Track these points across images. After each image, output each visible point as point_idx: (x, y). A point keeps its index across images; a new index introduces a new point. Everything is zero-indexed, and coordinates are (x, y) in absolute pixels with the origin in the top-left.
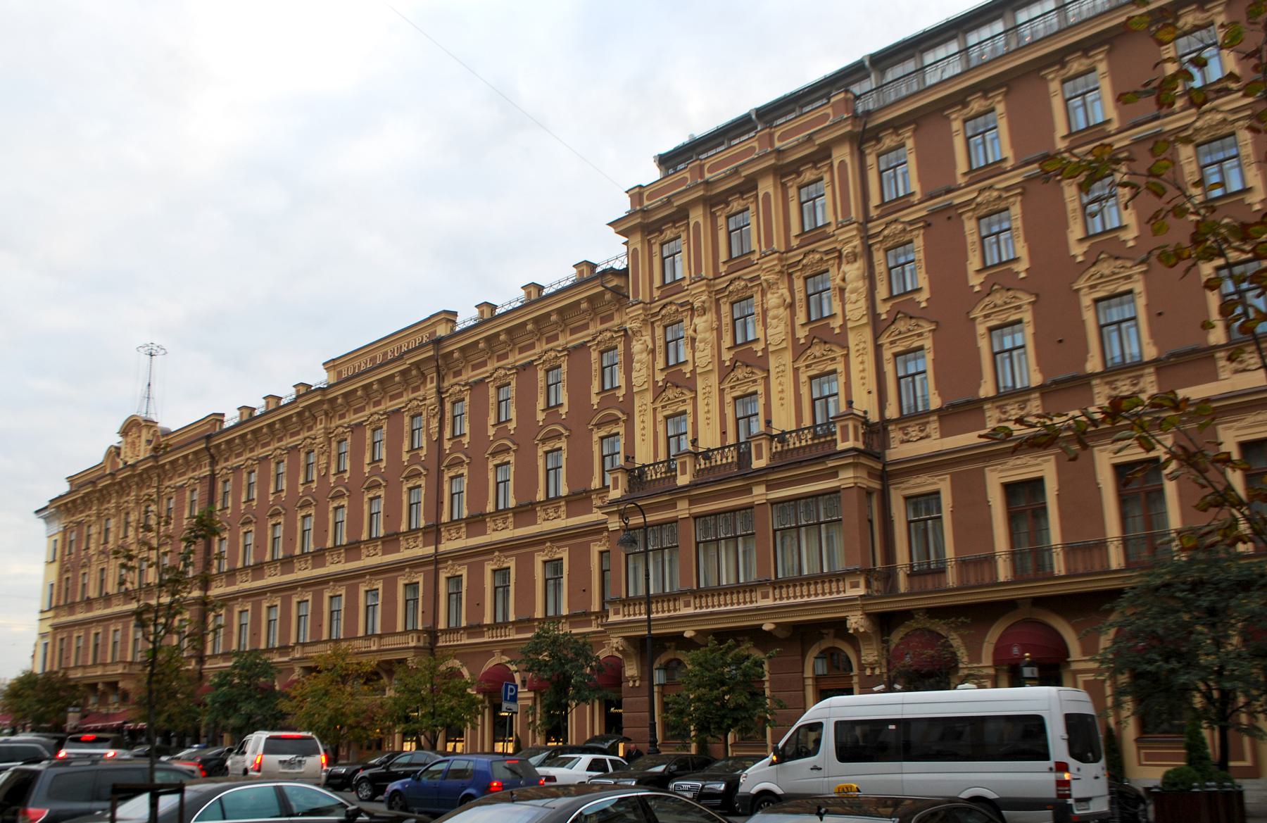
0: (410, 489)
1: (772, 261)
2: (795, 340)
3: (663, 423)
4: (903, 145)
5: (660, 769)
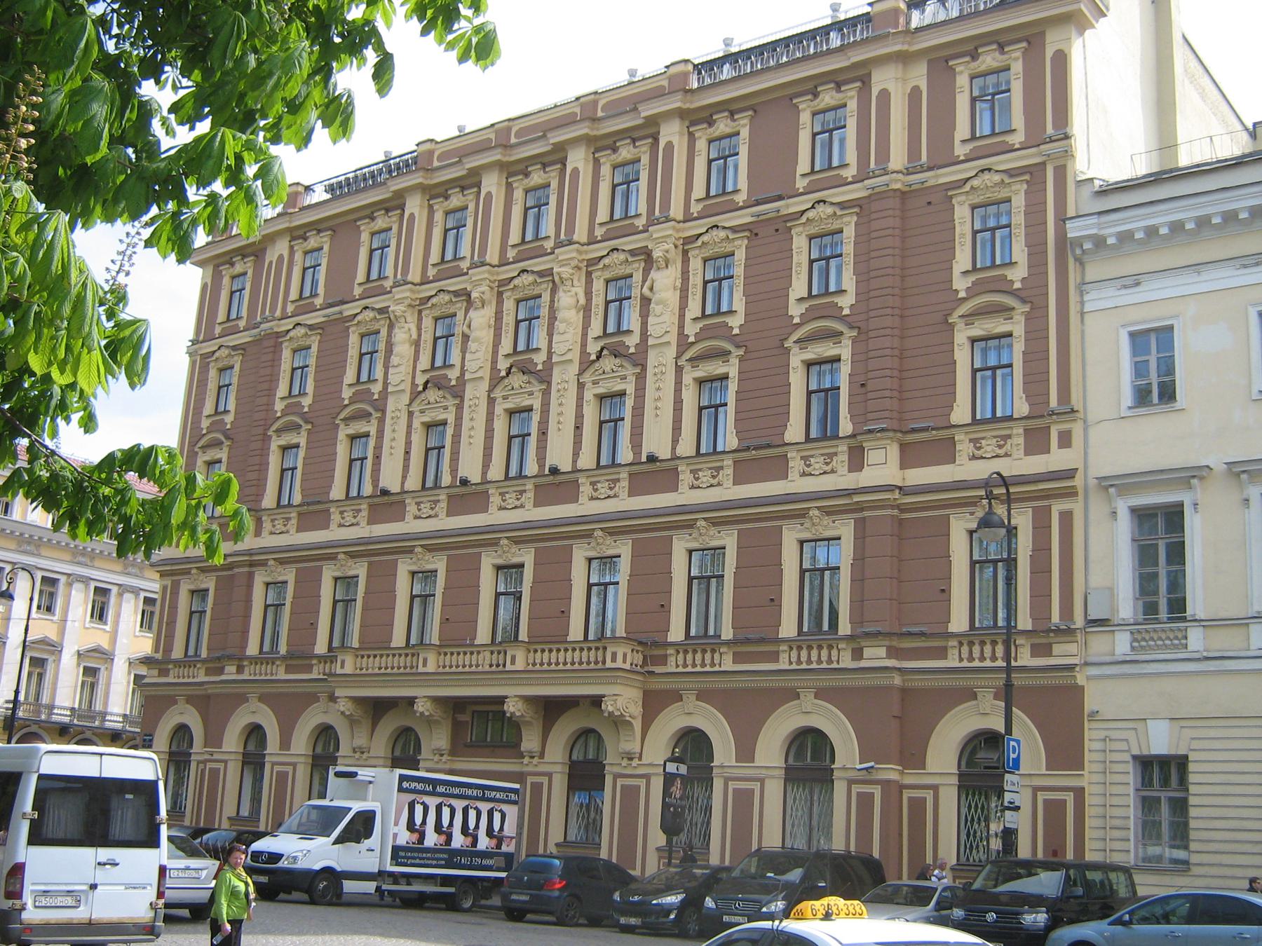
5: (636, 898)
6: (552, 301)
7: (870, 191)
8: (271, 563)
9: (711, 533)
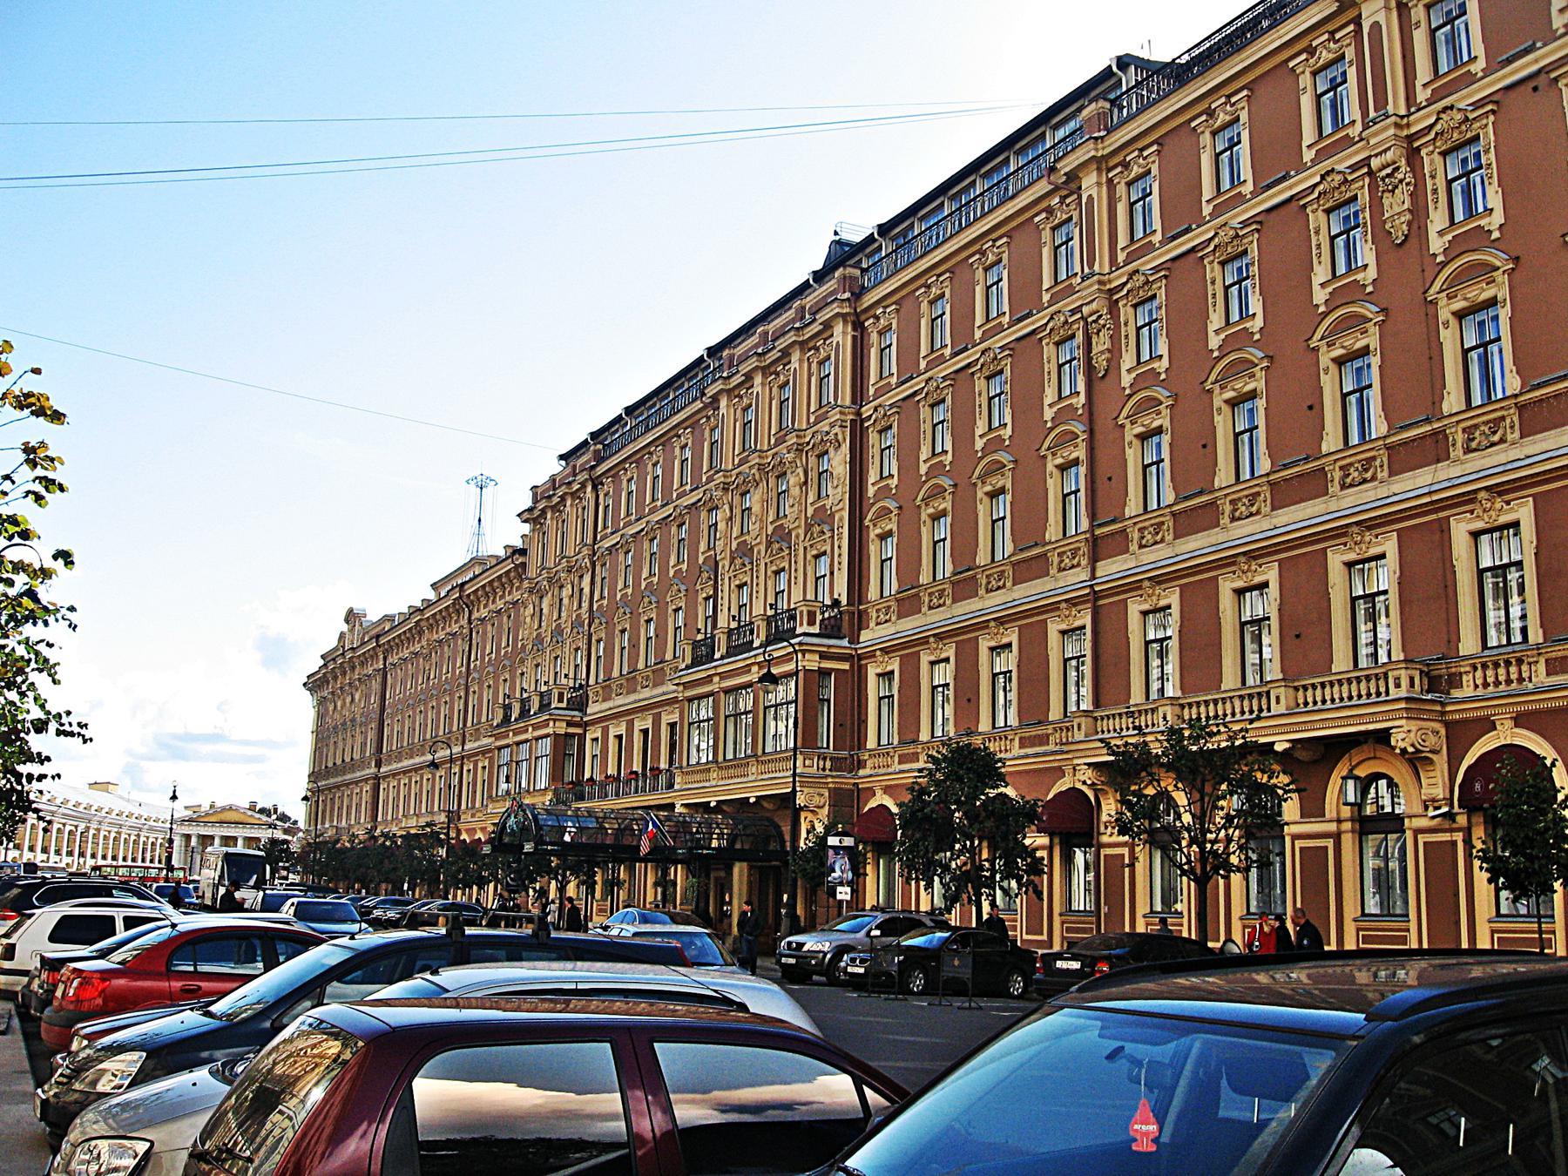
3: (929, 522)
9: (1498, 506)
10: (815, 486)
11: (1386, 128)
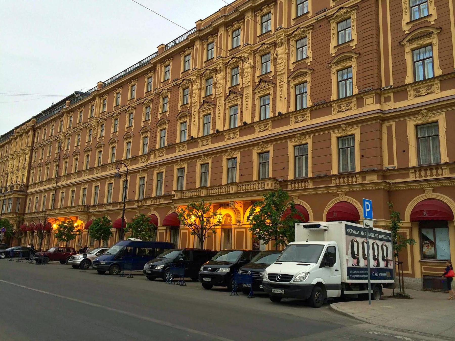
0: (181, 123)
1: (195, 72)
2: (289, 69)
4: (270, 12)
6: (242, 67)
7: (316, 20)
8: (158, 166)
9: (430, 115)
10: (408, 14)
11: (248, 48)
